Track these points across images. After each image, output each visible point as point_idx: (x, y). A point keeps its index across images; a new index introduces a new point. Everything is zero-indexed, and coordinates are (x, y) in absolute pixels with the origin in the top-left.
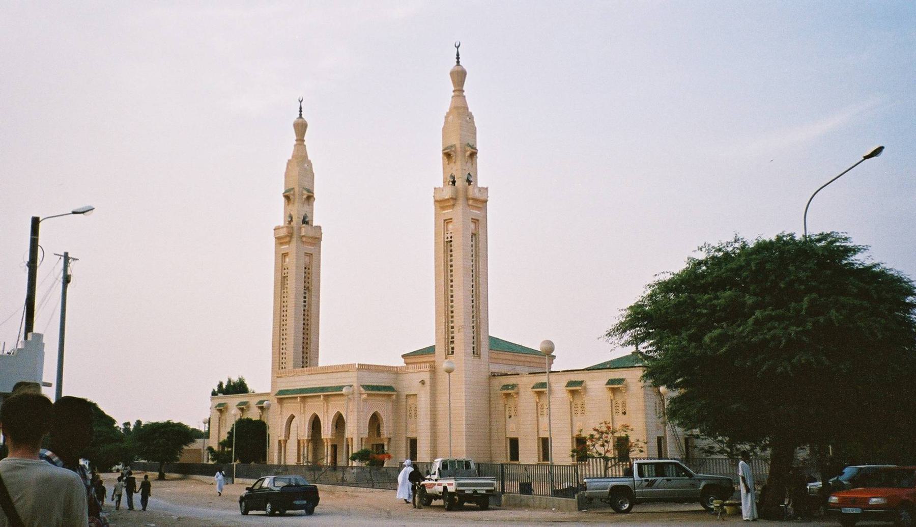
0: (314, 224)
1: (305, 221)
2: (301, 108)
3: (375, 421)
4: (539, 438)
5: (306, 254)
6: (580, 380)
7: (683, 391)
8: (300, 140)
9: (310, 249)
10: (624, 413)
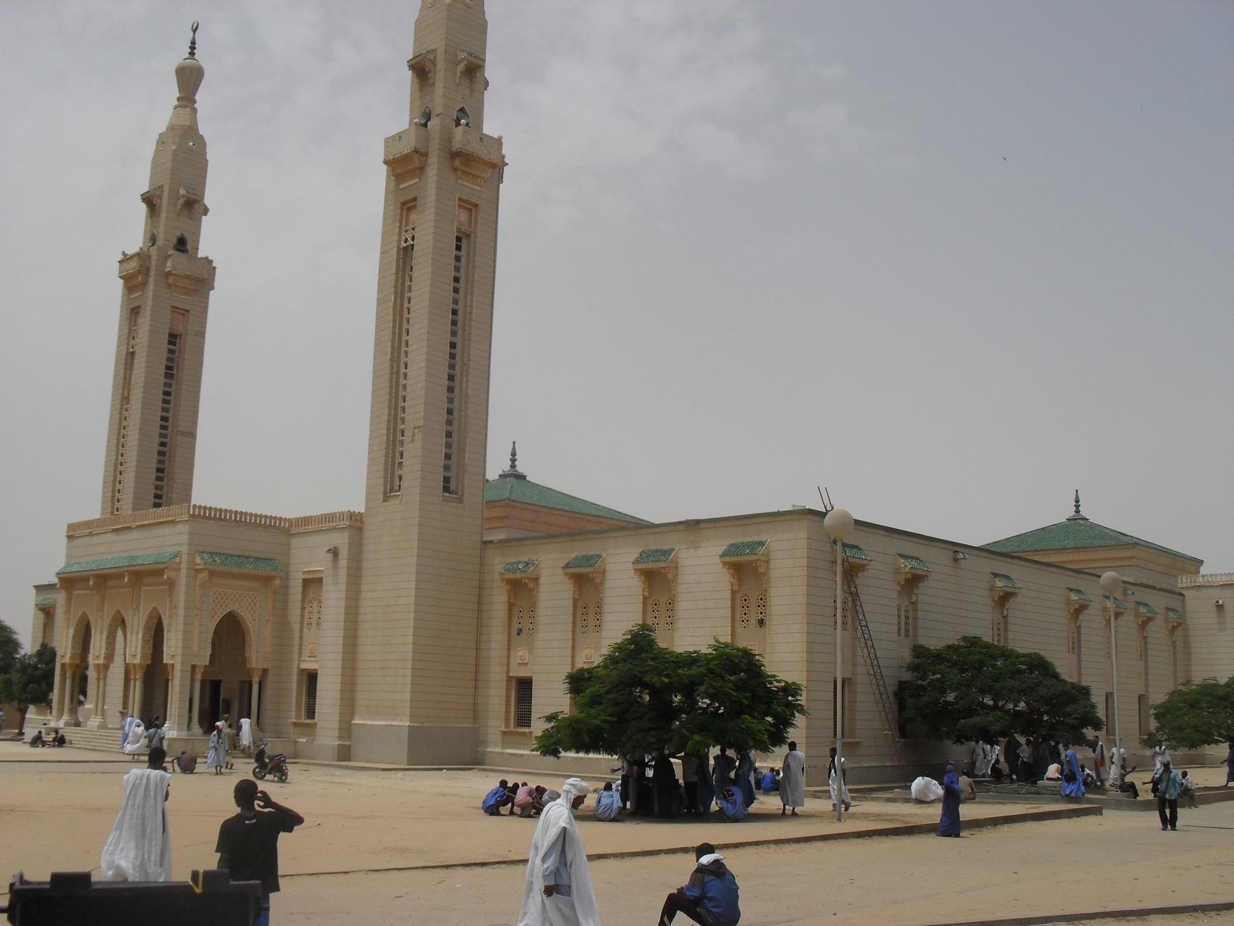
0: (201, 254)
1: (182, 245)
2: (193, 43)
3: (230, 633)
4: (509, 679)
5: (174, 309)
6: (666, 547)
7: (681, 781)
8: (187, 98)
9: (182, 301)
10: (761, 622)
